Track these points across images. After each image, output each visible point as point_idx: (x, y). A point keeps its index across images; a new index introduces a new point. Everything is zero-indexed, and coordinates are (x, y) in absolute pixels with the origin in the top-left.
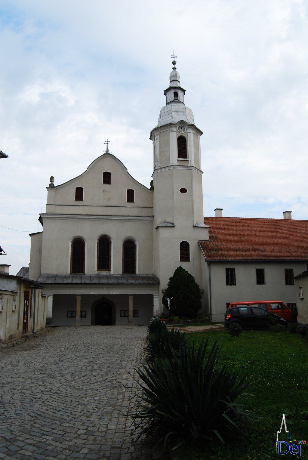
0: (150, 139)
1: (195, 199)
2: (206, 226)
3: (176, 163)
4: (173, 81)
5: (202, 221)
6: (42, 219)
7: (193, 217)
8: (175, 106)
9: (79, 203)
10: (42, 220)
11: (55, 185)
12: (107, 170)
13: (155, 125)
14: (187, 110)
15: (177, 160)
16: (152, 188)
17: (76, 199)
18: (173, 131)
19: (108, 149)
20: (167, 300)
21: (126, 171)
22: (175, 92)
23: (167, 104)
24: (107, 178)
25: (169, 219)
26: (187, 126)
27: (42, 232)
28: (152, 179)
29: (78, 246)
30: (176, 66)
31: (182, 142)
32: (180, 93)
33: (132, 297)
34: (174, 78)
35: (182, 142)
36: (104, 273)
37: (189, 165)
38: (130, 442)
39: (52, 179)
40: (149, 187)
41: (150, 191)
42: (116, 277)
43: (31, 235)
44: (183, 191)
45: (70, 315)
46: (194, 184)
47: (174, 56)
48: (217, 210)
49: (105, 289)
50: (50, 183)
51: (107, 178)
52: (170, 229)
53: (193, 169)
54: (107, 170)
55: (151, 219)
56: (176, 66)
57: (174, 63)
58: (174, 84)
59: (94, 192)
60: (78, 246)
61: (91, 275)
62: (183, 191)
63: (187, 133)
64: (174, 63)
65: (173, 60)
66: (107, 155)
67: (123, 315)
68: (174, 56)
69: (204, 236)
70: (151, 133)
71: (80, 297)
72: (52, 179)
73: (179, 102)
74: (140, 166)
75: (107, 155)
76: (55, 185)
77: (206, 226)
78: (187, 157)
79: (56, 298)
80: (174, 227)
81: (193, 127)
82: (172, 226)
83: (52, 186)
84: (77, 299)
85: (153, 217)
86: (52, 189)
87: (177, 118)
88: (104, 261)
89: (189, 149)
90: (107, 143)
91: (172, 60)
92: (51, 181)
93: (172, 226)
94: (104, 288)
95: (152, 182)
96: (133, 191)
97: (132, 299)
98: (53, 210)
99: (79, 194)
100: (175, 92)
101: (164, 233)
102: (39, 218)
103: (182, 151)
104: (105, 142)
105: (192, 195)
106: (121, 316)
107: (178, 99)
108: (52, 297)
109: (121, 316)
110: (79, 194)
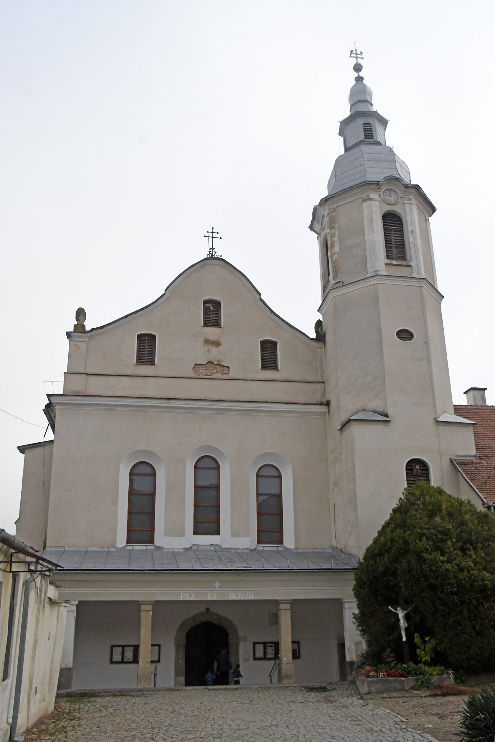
0: (311, 228)
1: (434, 356)
3: (385, 273)
4: (359, 101)
6: (53, 411)
10: (52, 414)
11: (88, 328)
12: (213, 293)
13: (325, 194)
15: (386, 264)
16: (321, 337)
17: (137, 362)
19: (213, 249)
20: (397, 614)
21: (258, 298)
23: (346, 149)
24: (212, 313)
25: (376, 404)
26: (403, 189)
27: (53, 440)
28: (320, 317)
29: (143, 475)
31: (393, 222)
33: (288, 606)
34: (360, 96)
35: (393, 222)
37: (414, 275)
39: (80, 314)
40: (313, 335)
41: (314, 343)
42: (240, 554)
43: (22, 449)
44: (405, 335)
45: (117, 657)
48: (471, 393)
49: (217, 584)
50: (76, 323)
51: (212, 313)
52: (378, 428)
54: (213, 293)
55: (318, 410)
57: (358, 68)
58: (361, 108)
59: (180, 349)
60: (143, 475)
61: (175, 550)
62: (405, 335)
63: (404, 204)
64: (358, 68)
65: (356, 62)
66: (213, 259)
67: (260, 654)
69: (465, 445)
72: (80, 314)
74: (295, 294)
75: (213, 259)
76: (88, 328)
79: (85, 611)
80: (389, 421)
82: (384, 418)
83: (80, 328)
84: (142, 613)
85: (328, 404)
86: (80, 337)
88: (207, 519)
89: (411, 240)
90: (212, 234)
91: (354, 61)
93: (384, 418)
94: (215, 582)
95: (319, 324)
97: (289, 613)
98: (79, 384)
99: (146, 347)
102: (46, 406)
104: (207, 234)
105: (426, 343)
106: (255, 659)
107: (374, 137)
108: (74, 608)
109: (255, 659)
110: (146, 347)
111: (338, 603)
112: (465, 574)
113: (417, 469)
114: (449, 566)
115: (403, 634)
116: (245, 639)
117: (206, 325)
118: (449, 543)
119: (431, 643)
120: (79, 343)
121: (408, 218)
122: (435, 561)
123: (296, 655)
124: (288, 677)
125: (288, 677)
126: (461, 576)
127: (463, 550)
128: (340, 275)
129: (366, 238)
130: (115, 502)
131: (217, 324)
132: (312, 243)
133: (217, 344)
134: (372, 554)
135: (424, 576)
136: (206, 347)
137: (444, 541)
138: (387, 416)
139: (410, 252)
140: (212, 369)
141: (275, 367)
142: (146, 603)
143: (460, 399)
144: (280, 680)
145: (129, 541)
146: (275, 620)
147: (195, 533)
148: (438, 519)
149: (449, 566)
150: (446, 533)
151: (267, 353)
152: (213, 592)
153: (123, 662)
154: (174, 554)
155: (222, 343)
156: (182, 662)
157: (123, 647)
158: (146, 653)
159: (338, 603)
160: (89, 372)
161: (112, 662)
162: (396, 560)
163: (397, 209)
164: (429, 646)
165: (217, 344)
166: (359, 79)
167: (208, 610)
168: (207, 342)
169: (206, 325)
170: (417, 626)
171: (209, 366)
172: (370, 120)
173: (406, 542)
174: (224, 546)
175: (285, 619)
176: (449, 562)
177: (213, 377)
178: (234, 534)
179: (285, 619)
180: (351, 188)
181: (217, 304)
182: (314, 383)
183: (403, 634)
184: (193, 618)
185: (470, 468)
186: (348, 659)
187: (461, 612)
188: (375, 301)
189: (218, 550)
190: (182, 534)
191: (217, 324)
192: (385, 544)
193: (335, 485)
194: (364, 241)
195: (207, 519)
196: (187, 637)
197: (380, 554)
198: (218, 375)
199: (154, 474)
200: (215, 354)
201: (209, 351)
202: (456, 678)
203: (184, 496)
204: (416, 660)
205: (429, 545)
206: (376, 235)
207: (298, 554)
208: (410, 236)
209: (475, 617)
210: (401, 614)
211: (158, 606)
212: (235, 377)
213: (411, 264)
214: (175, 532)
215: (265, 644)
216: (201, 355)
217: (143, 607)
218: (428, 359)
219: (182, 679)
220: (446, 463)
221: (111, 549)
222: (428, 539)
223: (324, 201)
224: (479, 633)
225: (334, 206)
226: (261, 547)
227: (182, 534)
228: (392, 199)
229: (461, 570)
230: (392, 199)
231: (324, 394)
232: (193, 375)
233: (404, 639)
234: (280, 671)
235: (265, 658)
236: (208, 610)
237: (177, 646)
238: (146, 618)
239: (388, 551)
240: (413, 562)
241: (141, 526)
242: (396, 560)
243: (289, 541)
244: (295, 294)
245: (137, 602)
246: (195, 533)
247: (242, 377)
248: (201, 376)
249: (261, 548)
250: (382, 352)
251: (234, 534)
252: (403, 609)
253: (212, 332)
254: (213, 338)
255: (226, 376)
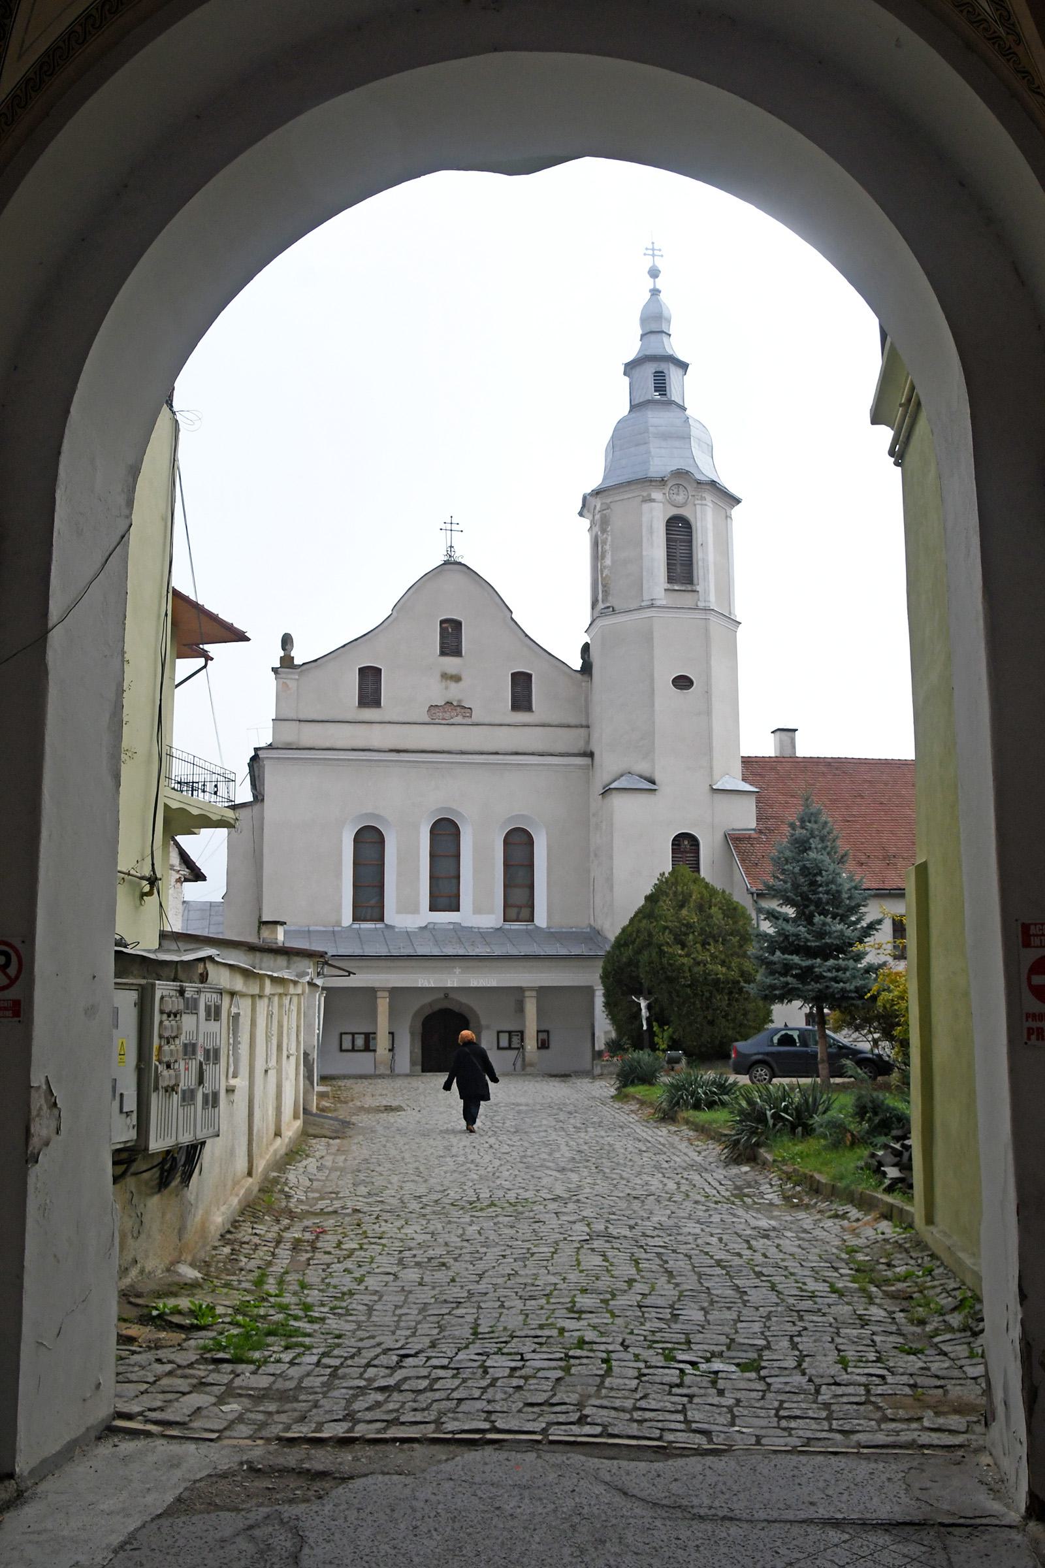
0: (581, 514)
1: (718, 707)
2: (747, 787)
3: (664, 602)
5: (738, 768)
6: (259, 767)
7: (711, 760)
8: (657, 419)
9: (369, 714)
12: (453, 612)
14: (694, 432)
16: (587, 668)
18: (653, 501)
22: (655, 374)
23: (633, 407)
24: (451, 637)
25: (642, 767)
29: (369, 843)
30: (660, 283)
31: (680, 530)
32: (673, 373)
33: (534, 994)
34: (654, 323)
35: (680, 530)
36: (444, 918)
37: (701, 604)
38: (1034, 935)
39: (287, 641)
40: (576, 663)
41: (579, 675)
42: (484, 935)
44: (683, 682)
45: (347, 1044)
46: (713, 663)
47: (653, 251)
49: (458, 971)
51: (451, 637)
52: (642, 798)
53: (713, 618)
54: (453, 612)
56: (660, 283)
57: (654, 273)
59: (411, 686)
60: (369, 843)
62: (683, 682)
64: (654, 273)
67: (504, 1042)
68: (653, 249)
69: (744, 816)
70: (585, 499)
71: (386, 994)
72: (287, 641)
73: (671, 403)
74: (555, 614)
75: (451, 564)
76: (296, 662)
77: (747, 787)
78: (695, 581)
81: (714, 485)
83: (287, 661)
87: (661, 463)
88: (445, 895)
89: (700, 556)
90: (450, 527)
91: (648, 263)
92: (284, 649)
95: (586, 649)
96: (529, 676)
97: (534, 1001)
98: (291, 734)
99: (370, 684)
100: (655, 374)
101: (624, 808)
103: (682, 566)
105: (708, 693)
110: (370, 684)
111: (589, 991)
112: (701, 968)
113: (685, 847)
114: (685, 960)
115: (644, 1023)
116: (488, 1027)
117: (443, 653)
118: (691, 937)
119: (669, 1030)
120: (288, 682)
121: (699, 524)
122: (673, 956)
123: (543, 1045)
124: (531, 1065)
125: (531, 1065)
126: (696, 969)
127: (704, 944)
128: (610, 598)
129: (644, 553)
130: (339, 875)
131: (457, 652)
132: (580, 532)
133: (457, 679)
134: (624, 940)
135: (662, 968)
136: (444, 684)
137: (686, 934)
138: (653, 783)
139: (699, 572)
140: (451, 712)
141: (529, 708)
142: (383, 989)
143: (762, 745)
144: (524, 1066)
145: (356, 919)
146: (520, 1009)
147: (433, 908)
148: (684, 912)
149: (685, 960)
150: (689, 926)
151: (519, 689)
152: (453, 979)
153: (353, 1050)
154: (408, 934)
155: (463, 677)
156: (418, 1051)
157: (353, 1034)
158: (382, 1042)
159: (589, 991)
160: (302, 717)
161: (341, 1050)
162: (639, 952)
163: (685, 512)
164: (666, 1035)
165: (457, 679)
166: (655, 292)
167: (446, 996)
168: (445, 676)
169: (443, 653)
170: (659, 1016)
171: (447, 707)
172: (663, 366)
173: (650, 935)
174: (464, 924)
175: (531, 1008)
176: (688, 955)
177: (452, 721)
178: (477, 911)
179: (531, 1008)
180: (629, 483)
181: (457, 625)
182: (576, 727)
183: (644, 1023)
184: (430, 1004)
185: (745, 846)
186: (597, 1048)
187: (694, 1003)
188: (648, 638)
189: (458, 929)
190: (416, 911)
191: (457, 652)
192: (631, 935)
193: (596, 855)
194: (641, 557)
195: (445, 895)
196: (424, 1024)
197: (626, 945)
198: (459, 719)
199: (382, 841)
200: (454, 692)
201: (447, 688)
202: (688, 1063)
203: (418, 867)
204: (654, 1047)
205: (668, 937)
206: (656, 552)
207: (552, 935)
208: (700, 549)
209: (708, 1008)
210: (643, 1004)
211: (395, 993)
212: (481, 720)
213: (698, 588)
214: (408, 908)
215: (510, 1033)
216: (437, 693)
217: (379, 994)
218: (709, 713)
219: (419, 1068)
220: (719, 837)
221: (336, 929)
222: (671, 932)
223: (597, 493)
224: (711, 1023)
225: (608, 501)
226: (508, 926)
227: (416, 911)
228: (680, 498)
229: (698, 964)
230: (680, 498)
231: (588, 742)
232: (427, 719)
233: (645, 1028)
234: (524, 1059)
235: (510, 1048)
236: (446, 996)
237: (412, 1034)
238: (383, 1005)
239: (633, 942)
240: (654, 954)
241: (369, 898)
242: (639, 952)
243: (541, 919)
244: (555, 614)
245: (373, 988)
246: (433, 908)
247: (487, 721)
248: (437, 721)
249: (507, 927)
250: (653, 705)
251: (477, 911)
252: (646, 999)
253: (451, 664)
254: (452, 671)
255: (468, 721)
